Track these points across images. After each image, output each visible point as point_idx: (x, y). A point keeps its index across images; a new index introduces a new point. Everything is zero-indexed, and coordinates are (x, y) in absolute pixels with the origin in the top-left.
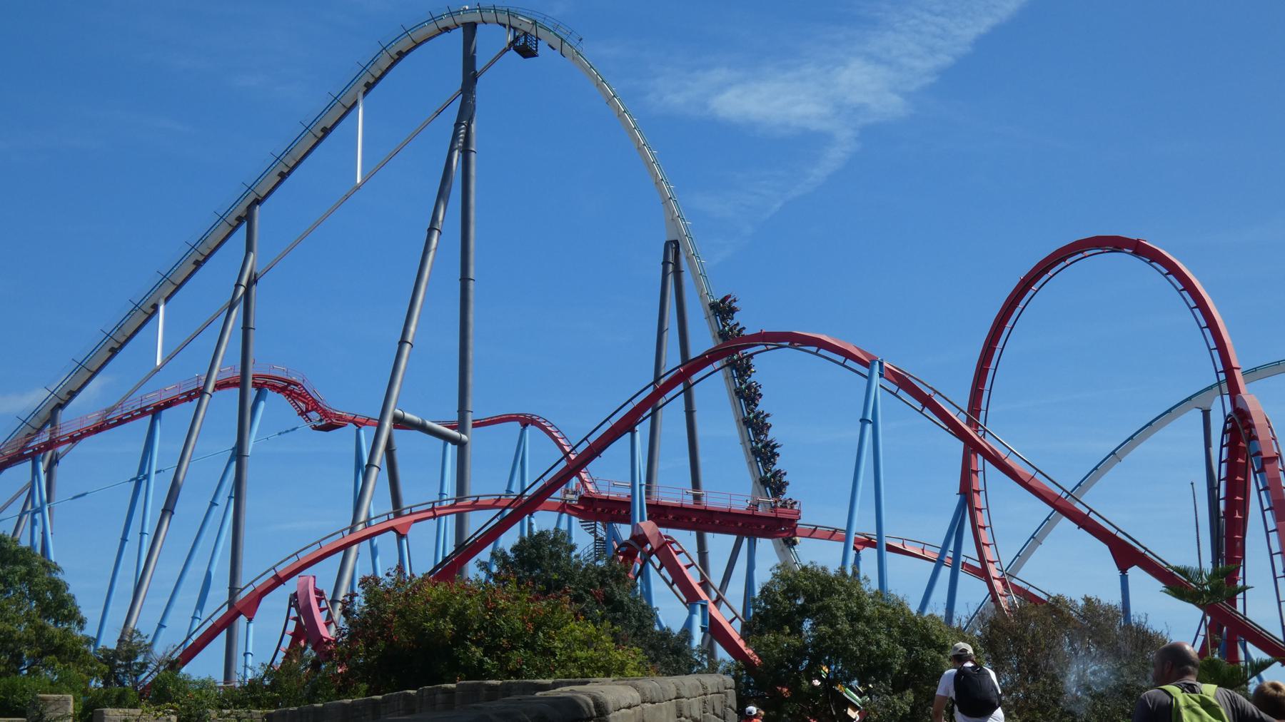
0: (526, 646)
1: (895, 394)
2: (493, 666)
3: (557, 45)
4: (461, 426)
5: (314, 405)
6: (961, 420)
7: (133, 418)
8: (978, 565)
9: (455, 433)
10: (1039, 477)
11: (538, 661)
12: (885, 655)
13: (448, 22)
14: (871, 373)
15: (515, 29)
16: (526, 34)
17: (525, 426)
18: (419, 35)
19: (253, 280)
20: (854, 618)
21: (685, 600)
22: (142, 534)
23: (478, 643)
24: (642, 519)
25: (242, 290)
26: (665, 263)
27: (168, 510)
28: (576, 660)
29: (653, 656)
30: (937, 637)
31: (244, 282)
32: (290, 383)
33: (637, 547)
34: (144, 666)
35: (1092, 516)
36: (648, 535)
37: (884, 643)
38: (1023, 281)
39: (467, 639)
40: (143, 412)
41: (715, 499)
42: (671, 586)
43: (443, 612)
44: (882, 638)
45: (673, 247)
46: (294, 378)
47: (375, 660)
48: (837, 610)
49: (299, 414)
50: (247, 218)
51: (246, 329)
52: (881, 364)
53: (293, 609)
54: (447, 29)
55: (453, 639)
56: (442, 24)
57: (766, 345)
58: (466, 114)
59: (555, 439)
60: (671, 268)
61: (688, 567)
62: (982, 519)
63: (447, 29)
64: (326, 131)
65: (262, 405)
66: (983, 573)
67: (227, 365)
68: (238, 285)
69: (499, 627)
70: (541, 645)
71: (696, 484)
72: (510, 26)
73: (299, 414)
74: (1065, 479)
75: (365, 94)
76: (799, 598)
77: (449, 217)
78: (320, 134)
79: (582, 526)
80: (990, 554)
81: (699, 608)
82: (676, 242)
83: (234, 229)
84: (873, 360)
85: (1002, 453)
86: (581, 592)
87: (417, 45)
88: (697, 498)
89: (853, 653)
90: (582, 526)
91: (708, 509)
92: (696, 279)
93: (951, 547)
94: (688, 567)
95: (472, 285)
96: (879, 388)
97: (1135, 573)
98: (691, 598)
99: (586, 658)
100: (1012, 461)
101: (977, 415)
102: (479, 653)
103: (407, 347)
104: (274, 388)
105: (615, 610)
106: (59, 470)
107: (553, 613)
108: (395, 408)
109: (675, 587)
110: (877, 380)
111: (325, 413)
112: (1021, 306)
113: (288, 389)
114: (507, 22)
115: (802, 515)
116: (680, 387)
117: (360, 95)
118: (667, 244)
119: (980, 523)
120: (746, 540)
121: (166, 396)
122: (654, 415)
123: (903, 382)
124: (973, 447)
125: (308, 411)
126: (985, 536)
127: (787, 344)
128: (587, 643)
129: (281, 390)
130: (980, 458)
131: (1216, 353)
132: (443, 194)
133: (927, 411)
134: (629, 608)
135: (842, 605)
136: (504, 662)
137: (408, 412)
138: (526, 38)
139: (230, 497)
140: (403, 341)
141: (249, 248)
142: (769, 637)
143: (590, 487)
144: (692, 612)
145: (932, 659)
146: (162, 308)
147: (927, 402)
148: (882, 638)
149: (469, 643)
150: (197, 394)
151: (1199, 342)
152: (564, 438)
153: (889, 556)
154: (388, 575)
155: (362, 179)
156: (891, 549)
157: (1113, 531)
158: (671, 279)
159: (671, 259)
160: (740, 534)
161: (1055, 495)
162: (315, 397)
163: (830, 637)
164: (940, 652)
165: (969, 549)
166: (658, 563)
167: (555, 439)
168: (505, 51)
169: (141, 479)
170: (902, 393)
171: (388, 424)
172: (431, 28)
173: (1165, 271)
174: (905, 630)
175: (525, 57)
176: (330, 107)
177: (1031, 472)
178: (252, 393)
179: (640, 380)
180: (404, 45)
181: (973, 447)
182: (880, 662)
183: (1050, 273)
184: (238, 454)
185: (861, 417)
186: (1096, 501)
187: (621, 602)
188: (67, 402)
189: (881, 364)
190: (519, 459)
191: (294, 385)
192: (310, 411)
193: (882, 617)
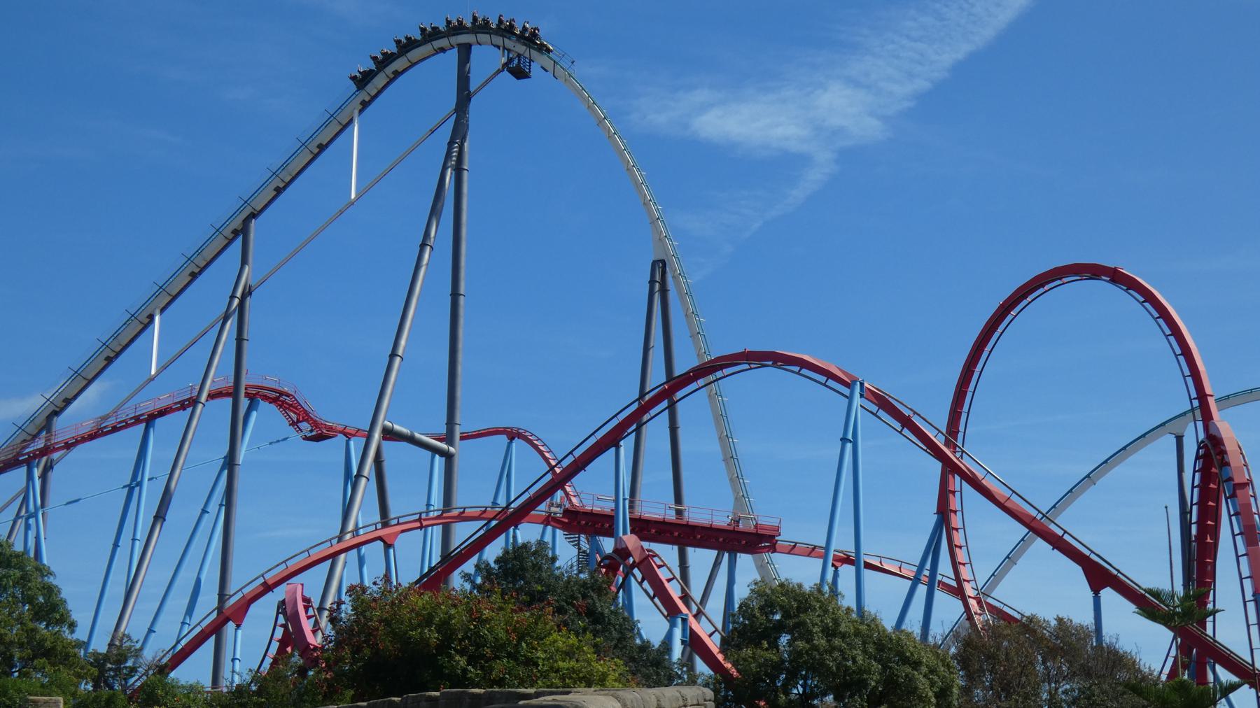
0: (509, 656)
1: (875, 415)
2: (477, 675)
3: (550, 67)
4: (449, 439)
5: (305, 416)
6: (940, 442)
7: (127, 426)
8: (954, 584)
9: (443, 446)
10: (1015, 498)
11: (521, 671)
12: (861, 671)
14: (852, 393)
15: (509, 51)
16: (519, 56)
17: (512, 439)
19: (247, 293)
22: (134, 540)
23: (462, 652)
24: (625, 533)
25: (236, 302)
26: (652, 282)
27: (160, 516)
28: (557, 671)
29: (634, 668)
30: (912, 654)
31: (239, 294)
32: (282, 394)
33: (620, 561)
34: (133, 670)
35: (1066, 537)
36: (630, 548)
37: (860, 658)
39: (451, 648)
40: (137, 420)
41: (696, 515)
42: (652, 599)
43: (428, 621)
45: (660, 267)
46: (286, 389)
47: (360, 667)
49: (290, 425)
51: (240, 340)
52: (862, 384)
53: (281, 616)
55: (438, 647)
58: (459, 133)
59: (541, 453)
60: (657, 286)
62: (958, 538)
64: (322, 148)
65: (254, 414)
67: (220, 375)
68: (233, 297)
69: (483, 637)
71: (678, 499)
72: (504, 48)
73: (290, 425)
74: (1040, 500)
75: (361, 111)
76: (776, 613)
77: (441, 233)
78: (316, 151)
79: (566, 538)
80: (965, 573)
81: (679, 621)
82: (663, 262)
83: (230, 242)
85: (980, 474)
88: (679, 513)
89: (829, 668)
90: (566, 538)
91: (690, 523)
93: (928, 566)
95: (462, 299)
97: (1108, 594)
98: (672, 611)
99: (568, 669)
100: (988, 482)
102: (462, 662)
104: (265, 398)
106: (53, 476)
109: (656, 600)
110: (857, 400)
111: (315, 424)
112: (1000, 330)
113: (280, 399)
114: (501, 43)
115: (782, 531)
116: (665, 404)
117: (356, 112)
118: (654, 264)
119: (956, 542)
120: (726, 555)
121: (161, 405)
122: (642, 394)
123: (883, 403)
124: (950, 468)
125: (299, 421)
126: (961, 556)
127: (770, 363)
128: (569, 654)
129: (274, 401)
130: (957, 478)
131: (1190, 380)
132: (435, 211)
133: (906, 432)
134: (609, 620)
135: (817, 620)
138: (519, 60)
139: (221, 505)
140: (393, 355)
141: (244, 261)
142: (747, 652)
143: (575, 500)
144: (673, 625)
145: (907, 676)
146: (157, 319)
147: (907, 423)
149: (453, 652)
150: (191, 403)
151: (1173, 369)
152: (550, 451)
153: (867, 573)
154: (375, 583)
156: (869, 566)
157: (1087, 552)
158: (657, 297)
159: (658, 278)
160: (721, 548)
161: (1030, 516)
162: (306, 408)
164: (914, 669)
165: (945, 568)
166: (639, 576)
167: (541, 453)
168: (499, 72)
169: (134, 485)
170: (882, 413)
171: (377, 435)
173: (1142, 299)
174: (880, 647)
175: (518, 78)
176: (326, 124)
177: (1007, 493)
178: (244, 403)
179: (625, 396)
181: (950, 468)
182: (856, 677)
183: (1029, 299)
184: (230, 462)
186: (1071, 524)
187: (602, 614)
188: (62, 409)
189: (862, 384)
190: (505, 472)
192: (301, 422)
193: (857, 633)
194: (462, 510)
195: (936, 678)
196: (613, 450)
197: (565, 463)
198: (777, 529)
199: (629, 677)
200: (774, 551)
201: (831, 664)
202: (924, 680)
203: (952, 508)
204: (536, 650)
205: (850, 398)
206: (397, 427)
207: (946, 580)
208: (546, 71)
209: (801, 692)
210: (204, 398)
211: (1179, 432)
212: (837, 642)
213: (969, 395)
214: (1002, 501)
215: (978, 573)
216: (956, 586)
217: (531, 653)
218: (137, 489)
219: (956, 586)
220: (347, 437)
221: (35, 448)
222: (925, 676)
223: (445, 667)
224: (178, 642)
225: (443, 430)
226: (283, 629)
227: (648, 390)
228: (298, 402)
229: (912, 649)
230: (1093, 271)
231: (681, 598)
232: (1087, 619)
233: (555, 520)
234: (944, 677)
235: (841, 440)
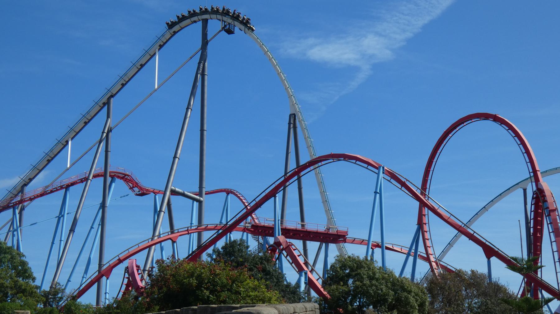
0: (228, 290)
1: (389, 181)
4: (200, 194)
5: (136, 185)
6: (418, 193)
7: (57, 190)
8: (425, 256)
9: (198, 197)
11: (233, 297)
12: (385, 295)
15: (225, 22)
16: (229, 24)
17: (228, 194)
19: (110, 130)
20: (371, 278)
21: (297, 270)
22: (61, 240)
23: (207, 289)
24: (279, 235)
25: (105, 135)
26: (290, 123)
27: (72, 230)
28: (249, 296)
30: (408, 287)
31: (106, 131)
32: (126, 175)
33: (276, 247)
34: (61, 298)
35: (475, 234)
37: (384, 290)
39: (202, 287)
40: (62, 187)
41: (311, 226)
42: (291, 264)
43: (192, 275)
44: (383, 287)
45: (293, 117)
47: (162, 296)
49: (129, 189)
50: (107, 103)
51: (107, 151)
52: (383, 168)
53: (126, 274)
57: (333, 159)
58: (203, 58)
59: (241, 200)
60: (292, 125)
61: (299, 256)
62: (427, 235)
64: (142, 66)
65: (113, 185)
66: (427, 259)
67: (98, 167)
68: (103, 132)
69: (216, 282)
70: (235, 290)
71: (302, 220)
72: (223, 21)
73: (129, 189)
74: (463, 218)
75: (159, 49)
77: (196, 103)
78: (140, 67)
79: (253, 238)
80: (430, 251)
81: (303, 274)
82: (294, 114)
83: (102, 108)
85: (436, 207)
86: (252, 267)
91: (297, 229)
92: (304, 133)
93: (414, 248)
94: (299, 256)
95: (205, 133)
96: (382, 178)
97: (494, 259)
98: (300, 269)
99: (254, 296)
100: (440, 211)
101: (425, 190)
102: (207, 293)
103: (177, 159)
104: (118, 177)
105: (266, 275)
106: (24, 213)
109: (293, 264)
110: (381, 175)
111: (141, 188)
113: (125, 178)
114: (221, 19)
115: (349, 233)
116: (296, 177)
117: (157, 50)
118: (290, 115)
120: (324, 244)
121: (72, 181)
122: (286, 174)
123: (393, 176)
124: (423, 204)
125: (133, 187)
126: (428, 243)
127: (343, 159)
128: (255, 289)
129: (122, 178)
130: (426, 209)
131: (529, 164)
132: (193, 93)
133: (403, 188)
134: (273, 274)
135: (366, 273)
136: (218, 297)
138: (229, 26)
139: (99, 225)
140: (175, 157)
141: (108, 117)
142: (334, 287)
143: (256, 221)
144: (301, 276)
145: (405, 297)
146: (70, 142)
147: (403, 184)
148: (383, 287)
149: (203, 289)
150: (86, 179)
151: (522, 160)
154: (168, 259)
155: (158, 86)
156: (387, 248)
157: (484, 241)
158: (292, 130)
159: (292, 122)
161: (459, 225)
162: (137, 181)
164: (408, 294)
165: (421, 249)
166: (285, 254)
167: (241, 200)
168: (220, 31)
169: (60, 216)
170: (392, 180)
171: (168, 193)
173: (507, 128)
174: (393, 284)
175: (229, 34)
176: (144, 55)
177: (449, 215)
178: (109, 179)
179: (278, 174)
181: (423, 204)
183: (457, 129)
184: (103, 206)
185: (375, 191)
186: (477, 228)
187: (269, 271)
188: (28, 183)
189: (383, 168)
191: (128, 176)
192: (134, 187)
193: (383, 278)
195: (418, 298)
197: (252, 205)
198: (347, 233)
199: (282, 299)
200: (345, 242)
202: (413, 299)
203: (425, 230)
204: (240, 287)
205: (378, 174)
206: (177, 189)
207: (421, 254)
208: (241, 30)
210: (91, 177)
211: (525, 188)
212: (374, 282)
213: (431, 172)
215: (436, 251)
217: (238, 289)
218: (62, 218)
221: (16, 200)
222: (413, 297)
223: (200, 296)
224: (81, 286)
226: (127, 279)
227: (282, 191)
229: (407, 285)
230: (486, 116)
231: (304, 264)
233: (248, 230)
234: (422, 297)
235: (374, 192)
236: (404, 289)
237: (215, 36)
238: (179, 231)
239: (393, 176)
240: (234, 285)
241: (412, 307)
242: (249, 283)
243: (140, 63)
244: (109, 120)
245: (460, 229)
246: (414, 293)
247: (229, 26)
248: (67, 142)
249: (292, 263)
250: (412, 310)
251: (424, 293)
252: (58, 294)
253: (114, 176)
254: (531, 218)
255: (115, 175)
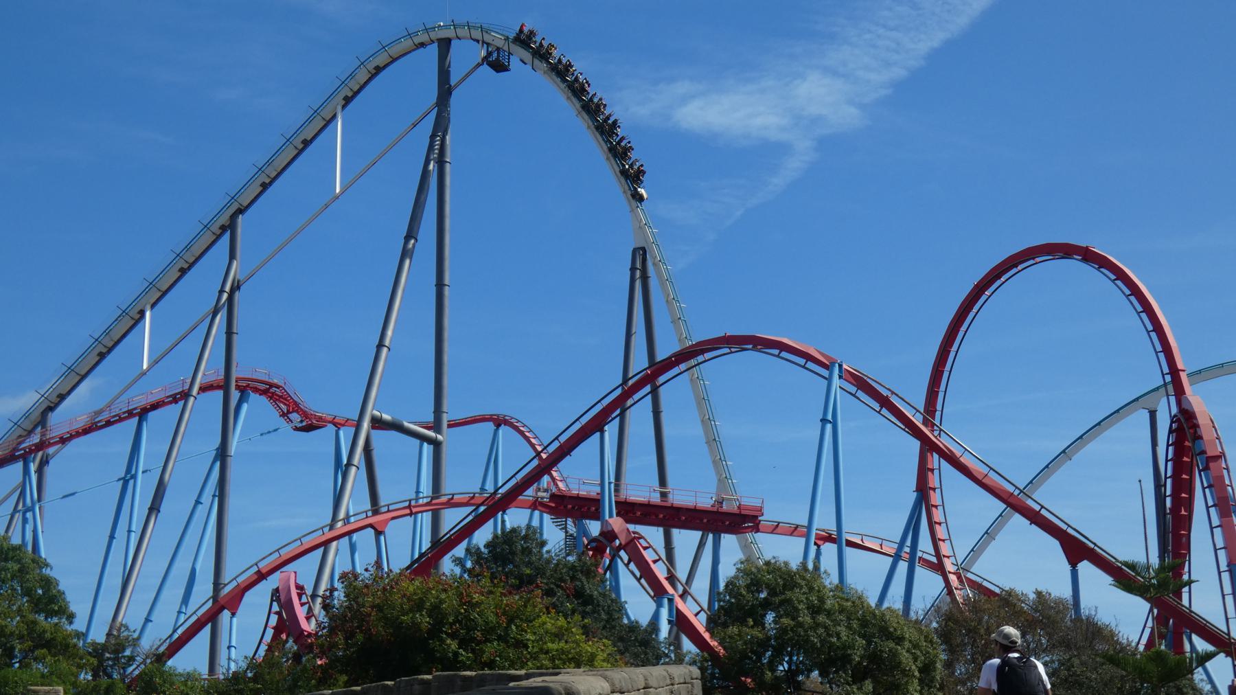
0: (500, 638)
1: (854, 395)
2: (468, 658)
4: (436, 427)
5: (295, 407)
6: (918, 421)
7: (121, 420)
8: (934, 560)
9: (431, 434)
10: (992, 475)
11: (511, 653)
12: (845, 647)
13: (423, 38)
15: (488, 44)
16: (498, 49)
17: (498, 426)
18: (395, 50)
19: (236, 287)
20: (815, 610)
22: (129, 531)
23: (453, 636)
24: (611, 516)
25: (225, 296)
26: (633, 269)
27: (154, 508)
28: (547, 652)
31: (228, 288)
32: (272, 385)
34: (131, 659)
35: (1043, 512)
38: (976, 286)
39: (442, 632)
40: (130, 414)
41: (680, 497)
42: (638, 580)
43: (419, 606)
44: (842, 630)
45: (640, 254)
46: (276, 381)
47: (354, 652)
48: (799, 603)
49: (281, 416)
51: (229, 333)
52: (840, 366)
53: (275, 604)
54: (422, 45)
55: (429, 632)
56: (417, 40)
57: (730, 348)
58: (441, 126)
59: (527, 439)
60: (638, 273)
61: (655, 562)
62: (938, 515)
63: (422, 45)
64: (306, 143)
65: (245, 407)
66: (939, 568)
67: (211, 369)
68: (221, 291)
69: (473, 620)
71: (663, 481)
72: (484, 42)
73: (281, 416)
74: (1017, 476)
75: (344, 107)
80: (945, 549)
81: (666, 601)
82: (644, 249)
83: (218, 237)
84: (833, 363)
85: (957, 452)
87: (394, 60)
88: (664, 495)
93: (908, 543)
94: (655, 562)
95: (447, 290)
96: (838, 388)
97: (1085, 567)
98: (658, 592)
99: (557, 650)
100: (966, 460)
101: (933, 415)
102: (454, 645)
103: (385, 350)
104: (256, 390)
105: (585, 604)
106: (49, 470)
107: (526, 607)
108: (372, 410)
110: (836, 382)
111: (305, 415)
112: (975, 310)
113: (270, 391)
114: (480, 38)
115: (765, 511)
116: (648, 388)
117: (339, 108)
118: (635, 251)
120: (711, 536)
121: (153, 399)
123: (862, 384)
124: (928, 446)
125: (289, 412)
126: (941, 532)
127: (750, 346)
128: (558, 636)
129: (263, 392)
130: (936, 456)
131: (1162, 356)
133: (884, 411)
134: (598, 602)
135: (803, 598)
136: (478, 654)
137: (385, 413)
138: (498, 54)
139: (214, 496)
140: (380, 345)
141: (232, 256)
142: (732, 630)
143: (561, 485)
144: (659, 605)
145: (890, 651)
146: (148, 314)
147: (885, 402)
149: (444, 636)
150: (185, 395)
151: (1146, 345)
154: (366, 570)
156: (851, 544)
157: (1064, 527)
158: (638, 284)
159: (638, 265)
160: (705, 529)
161: (1009, 492)
162: (296, 399)
163: (792, 629)
164: (897, 644)
165: (925, 545)
166: (626, 558)
167: (527, 439)
168: (479, 65)
170: (860, 394)
171: (366, 425)
172: (407, 44)
173: (1113, 277)
174: (864, 623)
176: (310, 120)
177: (985, 470)
178: (235, 395)
179: (609, 382)
180: (381, 60)
181: (928, 446)
182: (840, 653)
183: (1003, 279)
184: (222, 454)
185: (821, 417)
186: (1047, 499)
187: (591, 596)
188: (57, 405)
189: (840, 366)
190: (492, 459)
192: (291, 413)
193: (842, 610)
194: (647, 545)
195: (918, 653)
196: (598, 434)
197: (551, 449)
198: (760, 510)
199: (618, 657)
200: (758, 531)
201: (816, 640)
202: (907, 655)
204: (526, 632)
205: (829, 380)
207: (926, 556)
209: (786, 669)
211: (1152, 408)
212: (821, 618)
213: (946, 375)
214: (980, 478)
215: (957, 549)
216: (936, 562)
217: (521, 635)
218: (131, 482)
219: (936, 562)
220: (337, 427)
222: (907, 651)
225: (430, 418)
226: (277, 616)
228: (288, 393)
229: (895, 625)
230: (1065, 251)
231: (667, 579)
232: (1065, 592)
233: (542, 504)
234: (928, 653)
235: (821, 420)
236: (886, 632)
237: (467, 75)
238: (391, 508)
239: (862, 384)
240: (514, 627)
241: (906, 673)
242: (544, 623)
243: (302, 137)
244: (235, 264)
245: (1010, 500)
246: (910, 641)
247: (498, 54)
248: (142, 313)
249: (641, 577)
250: (906, 679)
251: (931, 642)
252: (124, 650)
253: (245, 389)
254: (1168, 476)
255: (248, 385)
